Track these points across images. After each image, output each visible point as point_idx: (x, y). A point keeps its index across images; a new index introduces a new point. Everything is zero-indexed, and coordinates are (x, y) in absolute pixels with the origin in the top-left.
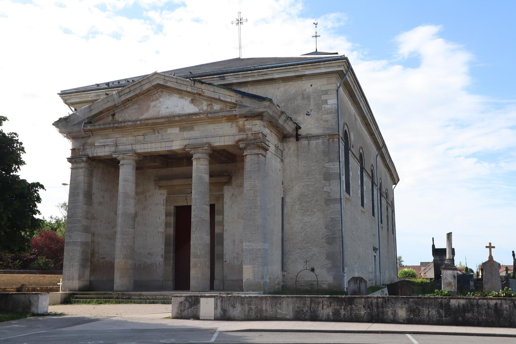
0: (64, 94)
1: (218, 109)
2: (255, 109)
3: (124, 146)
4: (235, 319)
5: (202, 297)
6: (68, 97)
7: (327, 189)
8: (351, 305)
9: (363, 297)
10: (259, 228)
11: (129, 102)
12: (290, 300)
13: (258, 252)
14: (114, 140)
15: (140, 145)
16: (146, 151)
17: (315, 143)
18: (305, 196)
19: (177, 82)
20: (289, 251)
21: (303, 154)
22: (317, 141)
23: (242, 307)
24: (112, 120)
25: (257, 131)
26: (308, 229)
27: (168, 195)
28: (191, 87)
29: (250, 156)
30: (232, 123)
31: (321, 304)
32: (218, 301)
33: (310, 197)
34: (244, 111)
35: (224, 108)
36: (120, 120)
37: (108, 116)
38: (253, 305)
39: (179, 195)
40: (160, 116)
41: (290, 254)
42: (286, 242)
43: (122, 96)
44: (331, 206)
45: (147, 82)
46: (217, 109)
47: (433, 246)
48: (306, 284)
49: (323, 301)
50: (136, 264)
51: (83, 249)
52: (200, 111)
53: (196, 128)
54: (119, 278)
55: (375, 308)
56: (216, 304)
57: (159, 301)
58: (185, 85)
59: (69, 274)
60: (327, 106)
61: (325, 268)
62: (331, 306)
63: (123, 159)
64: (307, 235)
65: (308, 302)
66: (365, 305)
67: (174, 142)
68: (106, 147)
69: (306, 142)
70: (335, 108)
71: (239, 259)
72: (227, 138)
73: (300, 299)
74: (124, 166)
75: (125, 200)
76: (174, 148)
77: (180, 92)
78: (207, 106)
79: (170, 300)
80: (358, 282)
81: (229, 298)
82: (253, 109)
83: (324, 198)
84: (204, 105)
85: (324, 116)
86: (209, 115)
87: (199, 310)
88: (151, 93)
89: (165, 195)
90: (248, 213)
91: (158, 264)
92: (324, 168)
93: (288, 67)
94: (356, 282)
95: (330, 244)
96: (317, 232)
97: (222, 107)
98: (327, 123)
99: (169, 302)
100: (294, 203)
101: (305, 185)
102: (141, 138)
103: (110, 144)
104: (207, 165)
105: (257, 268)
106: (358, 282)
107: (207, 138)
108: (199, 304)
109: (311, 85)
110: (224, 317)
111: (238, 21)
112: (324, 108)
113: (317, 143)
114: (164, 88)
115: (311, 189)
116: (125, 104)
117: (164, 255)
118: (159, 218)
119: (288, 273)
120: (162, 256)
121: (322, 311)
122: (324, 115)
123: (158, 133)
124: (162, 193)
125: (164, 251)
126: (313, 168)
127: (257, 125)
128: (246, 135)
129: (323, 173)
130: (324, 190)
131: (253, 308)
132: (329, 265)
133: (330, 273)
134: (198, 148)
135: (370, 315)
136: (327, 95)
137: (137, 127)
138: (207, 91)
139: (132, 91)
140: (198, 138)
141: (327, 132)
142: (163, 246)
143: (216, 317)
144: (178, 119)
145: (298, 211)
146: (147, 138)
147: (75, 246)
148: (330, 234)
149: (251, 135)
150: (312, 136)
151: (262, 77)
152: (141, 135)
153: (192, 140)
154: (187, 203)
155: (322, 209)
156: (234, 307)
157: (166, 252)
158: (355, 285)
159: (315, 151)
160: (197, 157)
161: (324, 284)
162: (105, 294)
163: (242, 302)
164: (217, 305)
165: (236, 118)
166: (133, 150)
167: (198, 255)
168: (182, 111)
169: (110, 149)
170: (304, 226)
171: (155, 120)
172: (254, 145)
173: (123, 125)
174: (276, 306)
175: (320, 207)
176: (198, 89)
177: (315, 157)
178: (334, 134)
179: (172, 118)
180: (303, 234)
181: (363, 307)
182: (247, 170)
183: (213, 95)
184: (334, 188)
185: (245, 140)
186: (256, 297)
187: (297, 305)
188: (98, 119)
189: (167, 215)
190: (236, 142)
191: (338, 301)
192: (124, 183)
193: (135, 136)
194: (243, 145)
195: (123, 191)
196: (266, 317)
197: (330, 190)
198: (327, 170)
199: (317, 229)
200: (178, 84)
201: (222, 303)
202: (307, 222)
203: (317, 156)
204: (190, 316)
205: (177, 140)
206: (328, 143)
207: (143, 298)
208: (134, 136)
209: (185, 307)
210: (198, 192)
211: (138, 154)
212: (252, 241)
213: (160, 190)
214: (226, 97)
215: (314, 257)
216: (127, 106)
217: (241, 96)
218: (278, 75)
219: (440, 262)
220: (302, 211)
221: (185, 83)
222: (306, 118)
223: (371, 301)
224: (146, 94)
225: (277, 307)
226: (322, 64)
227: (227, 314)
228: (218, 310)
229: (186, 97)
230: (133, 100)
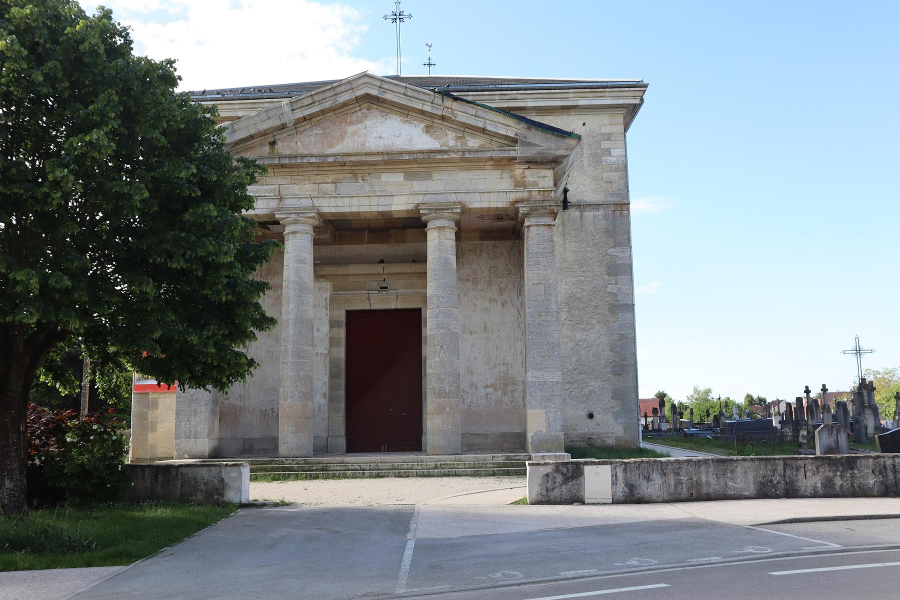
1: (476, 146)
2: (549, 150)
3: (297, 200)
4: (652, 500)
5: (586, 463)
7: (613, 289)
8: (852, 470)
9: (870, 457)
10: (555, 348)
11: (306, 123)
12: (748, 464)
14: (275, 189)
15: (328, 199)
16: (340, 210)
17: (592, 216)
19: (404, 94)
22: (596, 213)
23: (664, 478)
24: (269, 153)
25: (547, 187)
26: (582, 351)
27: (335, 290)
28: (431, 105)
29: (535, 228)
30: (502, 172)
31: (802, 470)
32: (618, 470)
34: (530, 153)
35: (488, 145)
36: (287, 152)
37: (262, 145)
39: (355, 292)
40: (367, 150)
43: (296, 111)
45: (347, 89)
46: (474, 146)
48: (580, 439)
49: (805, 464)
50: (273, 409)
52: (443, 147)
53: (436, 176)
54: (293, 434)
55: (891, 474)
56: (614, 476)
57: (389, 473)
58: (420, 100)
59: (188, 426)
60: (610, 159)
62: (819, 472)
64: (580, 361)
65: (780, 467)
66: (875, 469)
67: (395, 197)
68: (258, 200)
69: (578, 213)
70: (622, 162)
71: (466, 400)
72: (494, 197)
73: (766, 462)
74: (297, 235)
76: (394, 208)
77: (405, 111)
78: (456, 140)
79: (411, 471)
80: (835, 432)
82: (547, 149)
83: (607, 303)
84: (450, 137)
85: (605, 174)
86: (467, 155)
87: (583, 487)
88: (350, 109)
89: (329, 291)
90: (534, 323)
91: (316, 409)
92: (608, 256)
93: (553, 91)
94: (831, 434)
95: (618, 375)
96: (596, 357)
97: (483, 143)
98: (611, 185)
99: (409, 475)
101: (577, 282)
102: (330, 187)
103: (266, 195)
105: (553, 413)
106: (835, 432)
107: (457, 194)
108: (582, 478)
109: (584, 124)
110: (632, 498)
111: (396, 15)
113: (594, 217)
114: (374, 102)
115: (586, 287)
116: (298, 126)
117: (328, 394)
118: (318, 330)
120: (324, 395)
121: (804, 481)
122: (607, 172)
123: (363, 180)
124: (322, 288)
125: (328, 387)
126: (589, 255)
127: (546, 177)
128: (527, 193)
129: (605, 263)
130: (608, 290)
131: (684, 481)
132: (618, 408)
133: (619, 420)
134: (443, 209)
135: (884, 484)
137: (322, 167)
138: (462, 113)
139: (316, 104)
140: (440, 193)
141: (611, 199)
142: (326, 379)
143: (615, 498)
144: (408, 158)
146: (343, 188)
148: (618, 360)
149: (537, 194)
150: (586, 204)
152: (330, 181)
153: (430, 196)
154: (370, 305)
155: (605, 320)
156: (648, 479)
157: (331, 388)
158: (829, 437)
160: (440, 226)
161: (609, 437)
162: (270, 462)
163: (663, 471)
164: (616, 477)
165: (512, 163)
166: (314, 207)
167: (446, 392)
168: (407, 145)
169: (268, 204)
170: (575, 346)
171: (364, 157)
172: (545, 210)
173: (299, 161)
174: (724, 475)
176: (445, 109)
177: (593, 238)
178: (622, 202)
179: (397, 156)
180: (574, 359)
181: (871, 472)
183: (472, 122)
185: (527, 201)
186: (688, 461)
187: (761, 472)
188: (242, 149)
189: (333, 324)
190: (510, 204)
191: (829, 464)
192: (298, 265)
193: (319, 184)
194: (525, 209)
195: (297, 280)
196: (707, 494)
197: (618, 290)
199: (597, 351)
200: (407, 98)
201: (626, 473)
203: (595, 237)
204: (565, 498)
205: (401, 195)
206: (614, 217)
207: (352, 468)
208: (315, 183)
209: (555, 482)
210: (443, 285)
211: (321, 215)
212: (544, 370)
213: (319, 282)
214: (497, 126)
215: (593, 395)
216: (301, 129)
217: (525, 126)
218: (534, 103)
220: (572, 322)
221: (421, 96)
222: (576, 175)
223: (884, 462)
224: (340, 111)
225: (727, 477)
226: (608, 91)
227: (636, 492)
228: (618, 486)
229: (416, 122)
230: (313, 120)
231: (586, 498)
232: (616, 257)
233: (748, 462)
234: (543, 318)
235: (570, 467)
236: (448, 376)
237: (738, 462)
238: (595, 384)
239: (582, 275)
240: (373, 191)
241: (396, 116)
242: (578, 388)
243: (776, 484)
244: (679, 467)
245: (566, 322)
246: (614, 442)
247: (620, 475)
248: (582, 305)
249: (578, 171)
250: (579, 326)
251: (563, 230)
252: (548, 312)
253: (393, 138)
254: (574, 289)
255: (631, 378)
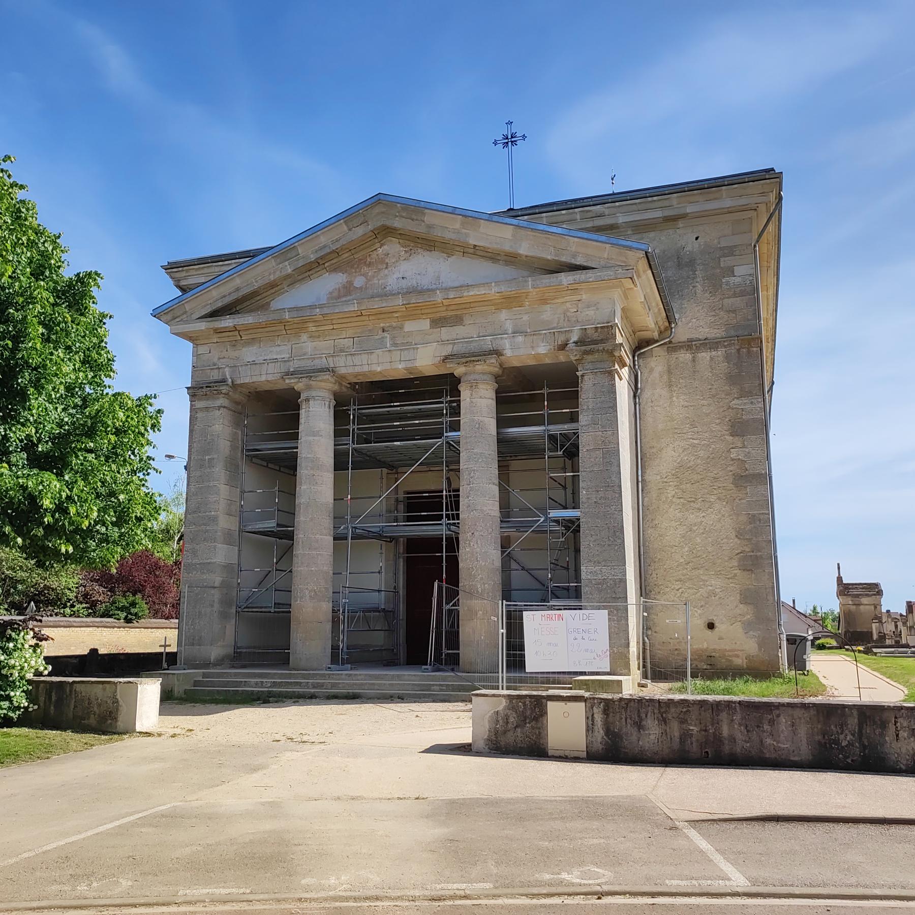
0: (171, 268)
6: (184, 274)
13: (617, 586)
17: (708, 358)
18: (689, 468)
20: (655, 585)
21: (681, 381)
22: (714, 353)
26: (698, 538)
33: (700, 470)
38: (693, 723)
41: (659, 592)
42: (649, 566)
44: (748, 490)
47: (840, 579)
48: (697, 657)
51: (221, 579)
56: (590, 718)
61: (740, 623)
63: (309, 388)
64: (694, 551)
68: (269, 364)
69: (688, 356)
70: (751, 283)
75: (314, 475)
81: (627, 704)
83: (730, 473)
98: (734, 315)
100: (665, 484)
101: (687, 446)
104: (493, 399)
109: (697, 238)
112: (728, 283)
113: (712, 358)
119: (655, 632)
122: (728, 298)
129: (727, 419)
130: (732, 456)
131: (695, 732)
132: (749, 617)
136: (733, 258)
145: (674, 500)
147: (206, 571)
148: (748, 550)
151: (591, 222)
156: (639, 726)
159: (710, 375)
161: (737, 656)
163: (662, 716)
164: (593, 720)
170: (687, 532)
175: (723, 491)
177: (710, 387)
182: (585, 407)
184: (753, 452)
198: (737, 414)
201: (607, 715)
202: (695, 523)
204: (520, 747)
215: (713, 598)
219: (854, 607)
220: (682, 500)
222: (686, 306)
228: (596, 734)
231: (549, 748)
232: (743, 411)
233: (798, 709)
234: (601, 494)
235: (528, 702)
236: (481, 571)
237: (780, 707)
238: (716, 583)
239: (695, 437)
240: (395, 344)
241: (422, 250)
242: (693, 588)
243: (846, 746)
244: (687, 711)
245: (674, 500)
246: (745, 663)
247: (599, 718)
248: (696, 477)
249: (688, 301)
250: (692, 504)
251: (669, 379)
252: (608, 486)
253: (419, 277)
254: (685, 456)
255: (766, 575)
